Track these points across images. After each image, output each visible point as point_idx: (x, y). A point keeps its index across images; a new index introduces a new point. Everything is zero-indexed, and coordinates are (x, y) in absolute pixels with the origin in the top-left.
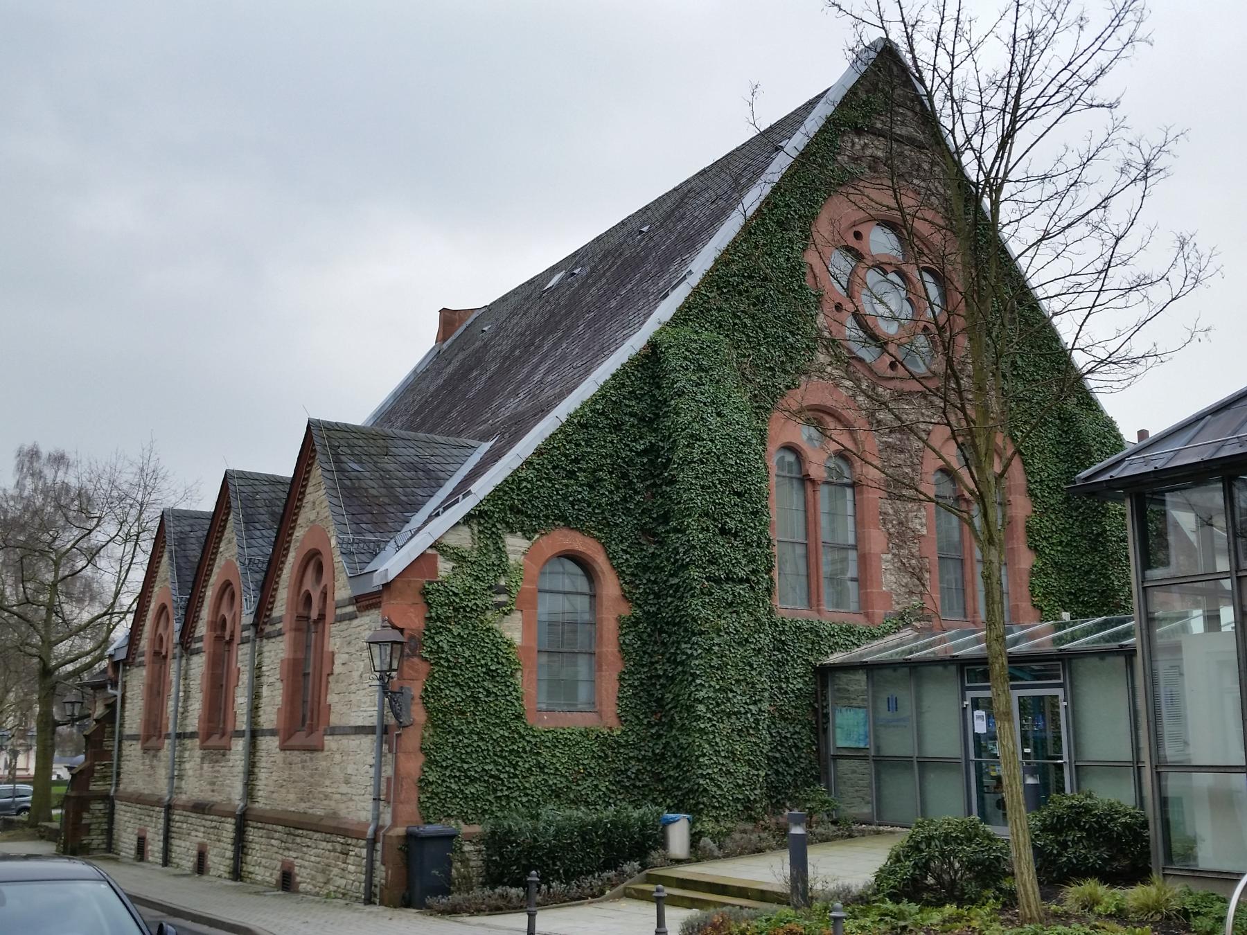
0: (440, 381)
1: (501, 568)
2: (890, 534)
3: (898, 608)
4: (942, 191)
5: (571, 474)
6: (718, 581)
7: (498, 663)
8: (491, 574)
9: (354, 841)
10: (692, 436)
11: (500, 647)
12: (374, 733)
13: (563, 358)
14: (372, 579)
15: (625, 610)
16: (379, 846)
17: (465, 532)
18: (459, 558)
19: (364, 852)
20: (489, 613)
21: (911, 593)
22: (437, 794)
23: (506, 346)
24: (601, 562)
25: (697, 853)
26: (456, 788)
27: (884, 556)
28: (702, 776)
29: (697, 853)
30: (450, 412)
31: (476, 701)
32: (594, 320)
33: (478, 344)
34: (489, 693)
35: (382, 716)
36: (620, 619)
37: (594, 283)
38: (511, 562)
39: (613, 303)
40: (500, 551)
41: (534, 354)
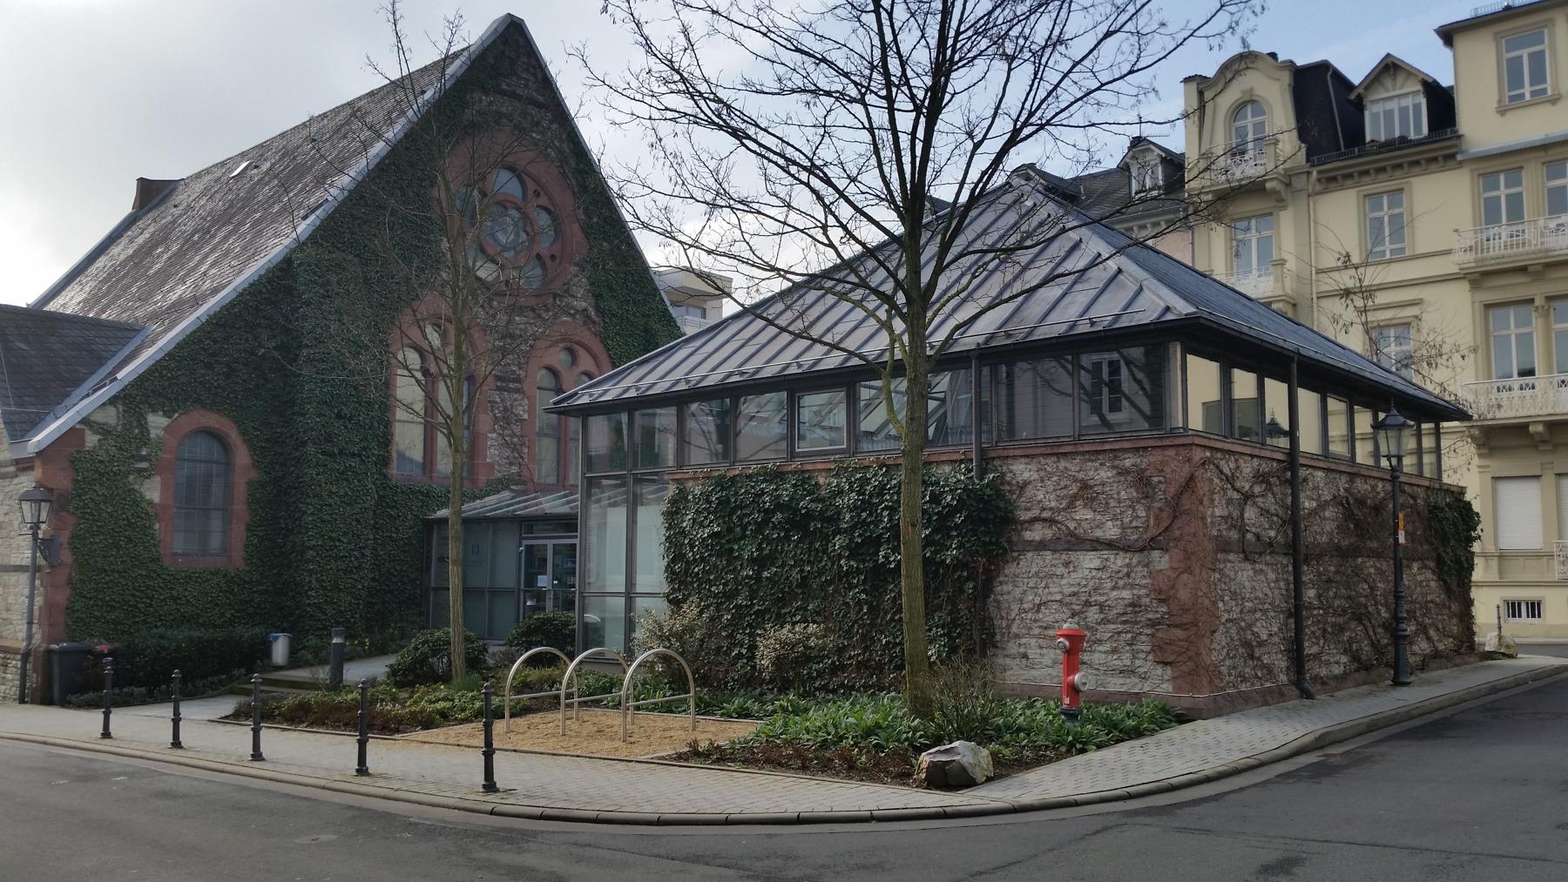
0: (130, 252)
1: (144, 438)
2: (496, 418)
3: (499, 475)
4: (558, 144)
5: (209, 366)
6: (331, 455)
7: (138, 517)
8: (134, 446)
9: (12, 656)
10: (315, 339)
11: (137, 501)
12: (28, 571)
13: (226, 254)
14: (26, 447)
15: (254, 475)
16: (31, 659)
17: (112, 411)
18: (103, 430)
19: (19, 664)
20: (131, 478)
21: (511, 464)
22: (82, 619)
23: (189, 228)
24: (234, 436)
25: (294, 661)
26: (99, 614)
27: (490, 435)
28: (309, 605)
29: (294, 661)
30: (131, 287)
31: (118, 547)
32: (257, 222)
33: (169, 218)
34: (130, 540)
35: (34, 558)
36: (249, 483)
37: (267, 184)
38: (152, 436)
39: (276, 208)
40: (144, 427)
41: (208, 242)
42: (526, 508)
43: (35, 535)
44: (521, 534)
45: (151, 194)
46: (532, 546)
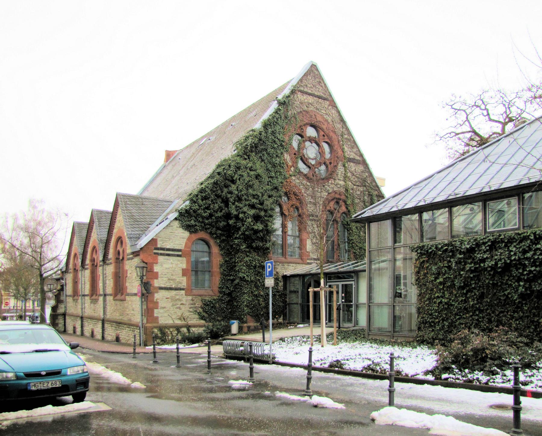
42: (329, 268)
43: (141, 281)
44: (326, 280)
45: (169, 155)
46: (346, 285)
